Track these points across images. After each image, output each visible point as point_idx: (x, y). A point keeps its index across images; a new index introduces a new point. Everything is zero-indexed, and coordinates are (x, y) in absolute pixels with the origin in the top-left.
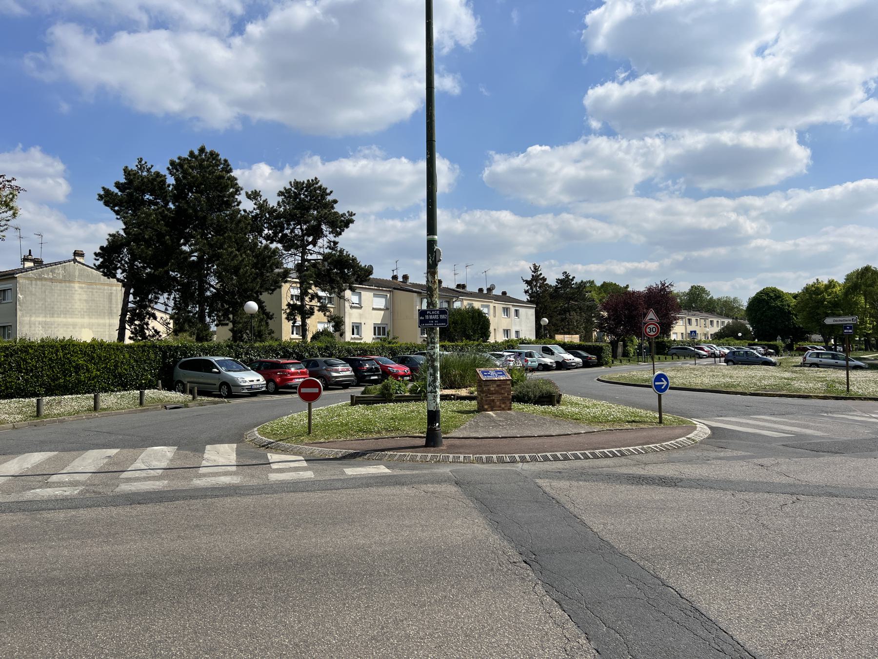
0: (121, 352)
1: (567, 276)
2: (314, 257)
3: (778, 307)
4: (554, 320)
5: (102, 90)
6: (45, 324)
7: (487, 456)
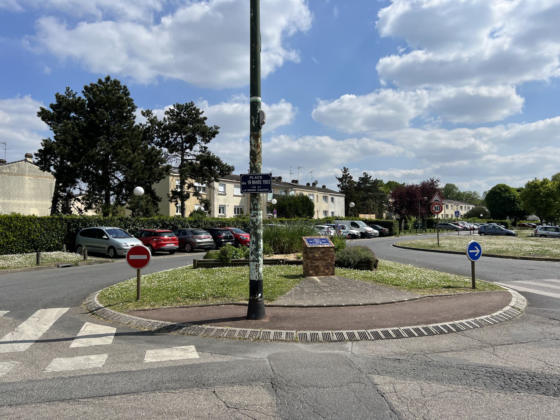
0: (34, 223)
1: (366, 176)
2: (191, 157)
3: (507, 197)
4: (357, 204)
5: (70, 59)
6: (4, 204)
7: (312, 332)
